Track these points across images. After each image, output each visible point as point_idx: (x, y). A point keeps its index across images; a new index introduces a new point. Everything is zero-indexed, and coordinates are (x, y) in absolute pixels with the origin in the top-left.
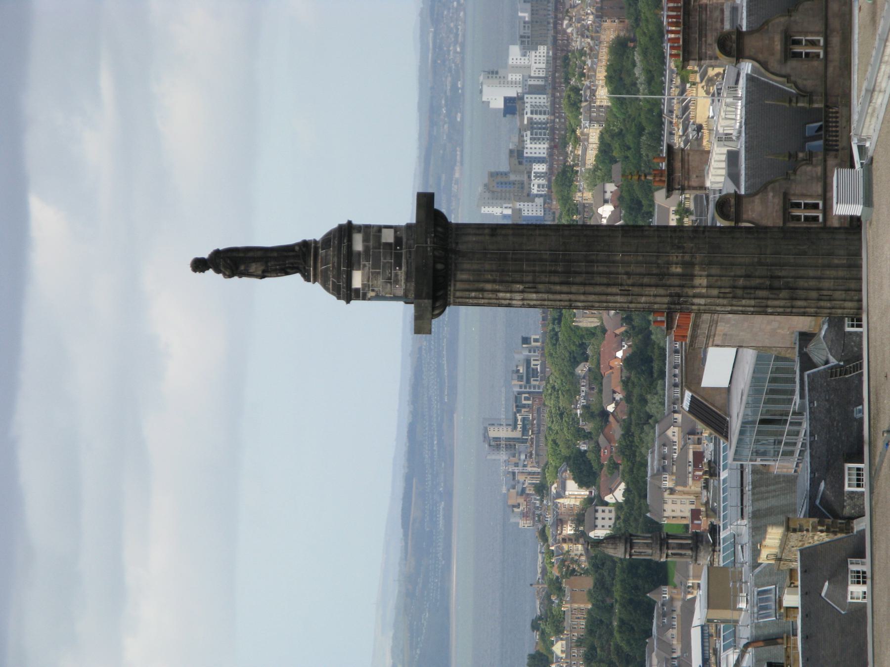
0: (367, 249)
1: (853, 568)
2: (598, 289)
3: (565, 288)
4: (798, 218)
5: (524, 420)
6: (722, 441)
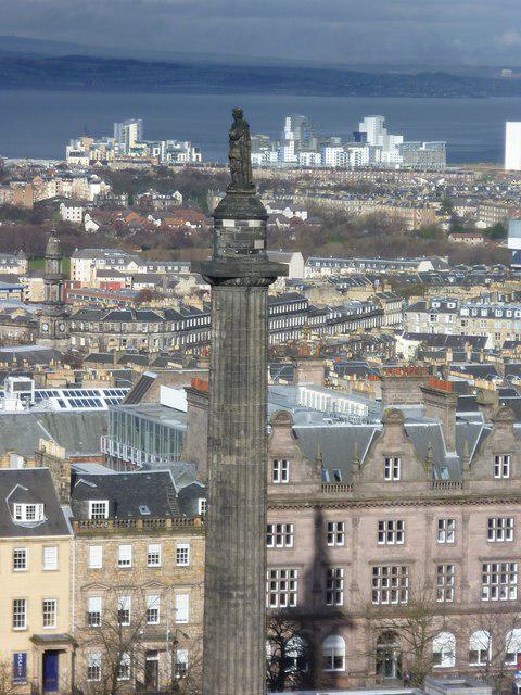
0: (251, 229)
1: (37, 506)
2: (222, 389)
3: (223, 367)
4: (276, 465)
5: (142, 149)
6: (127, 389)
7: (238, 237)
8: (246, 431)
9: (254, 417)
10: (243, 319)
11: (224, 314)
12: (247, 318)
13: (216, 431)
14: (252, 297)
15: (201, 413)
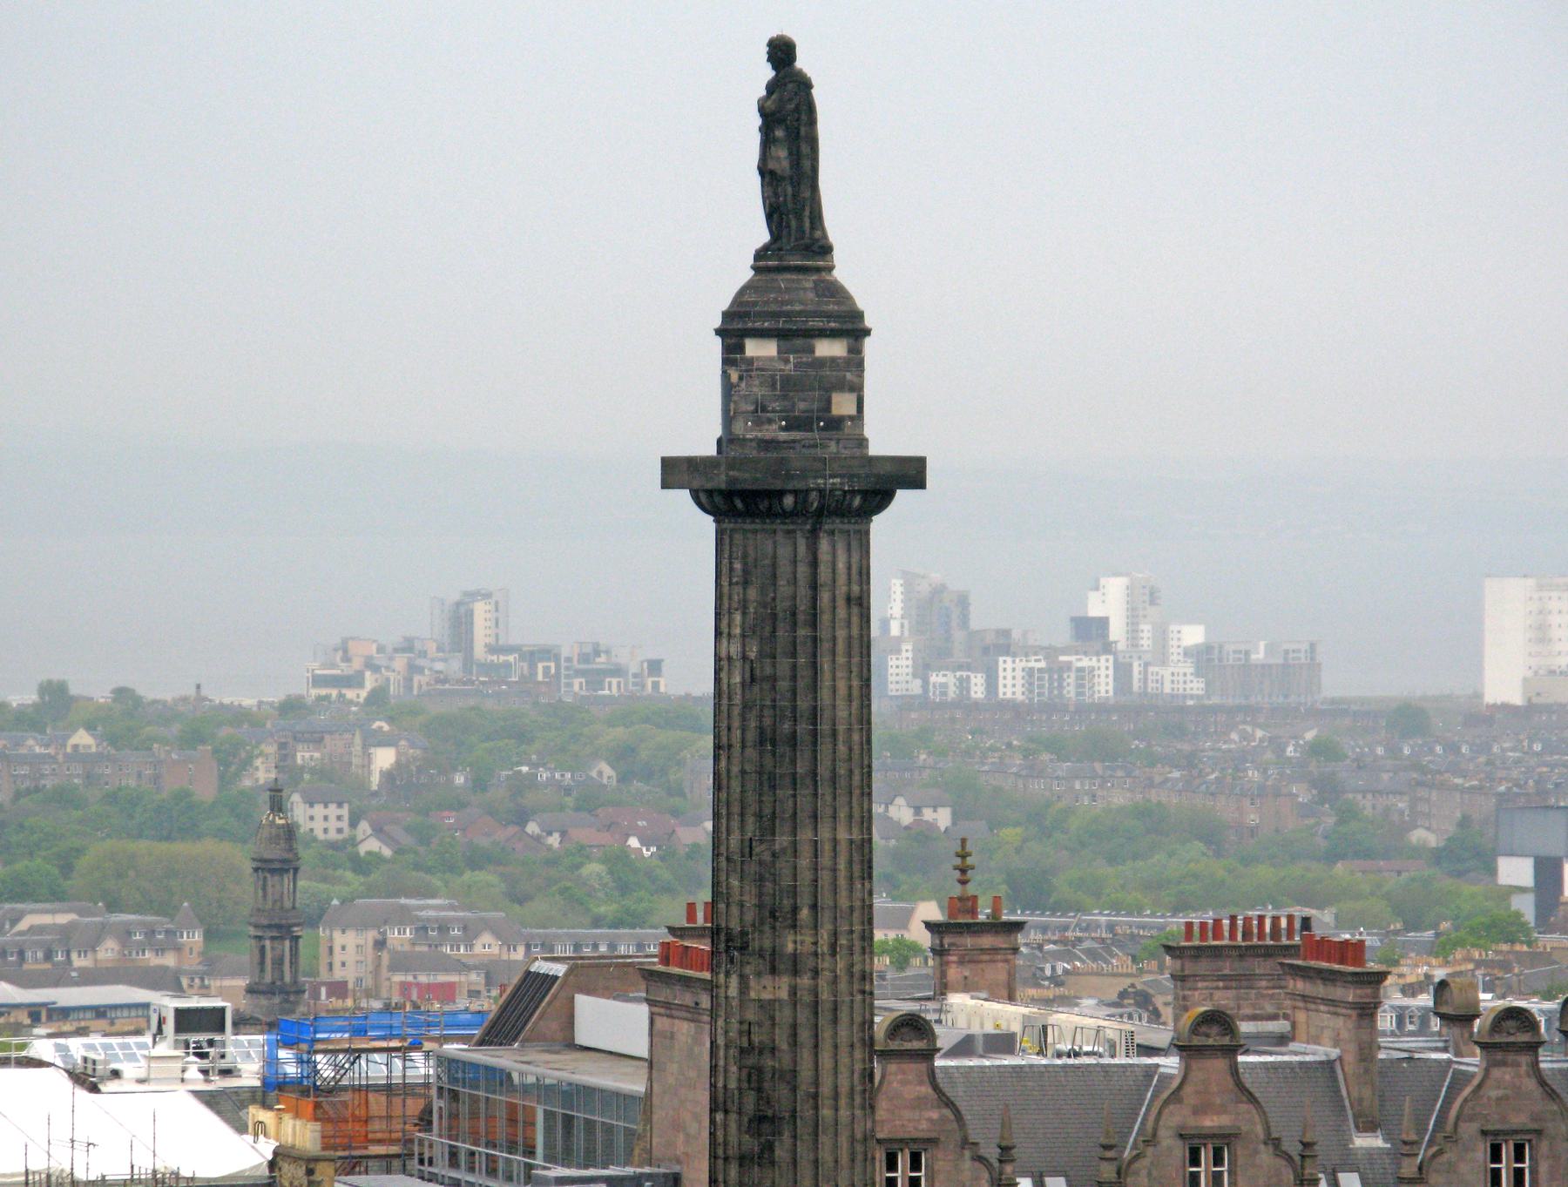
0: (822, 363)
2: (751, 797)
3: (752, 736)
7: (788, 385)
8: (814, 907)
9: (834, 870)
10: (803, 606)
11: (752, 593)
12: (814, 599)
13: (735, 910)
14: (824, 545)
15: (684, 1029)
